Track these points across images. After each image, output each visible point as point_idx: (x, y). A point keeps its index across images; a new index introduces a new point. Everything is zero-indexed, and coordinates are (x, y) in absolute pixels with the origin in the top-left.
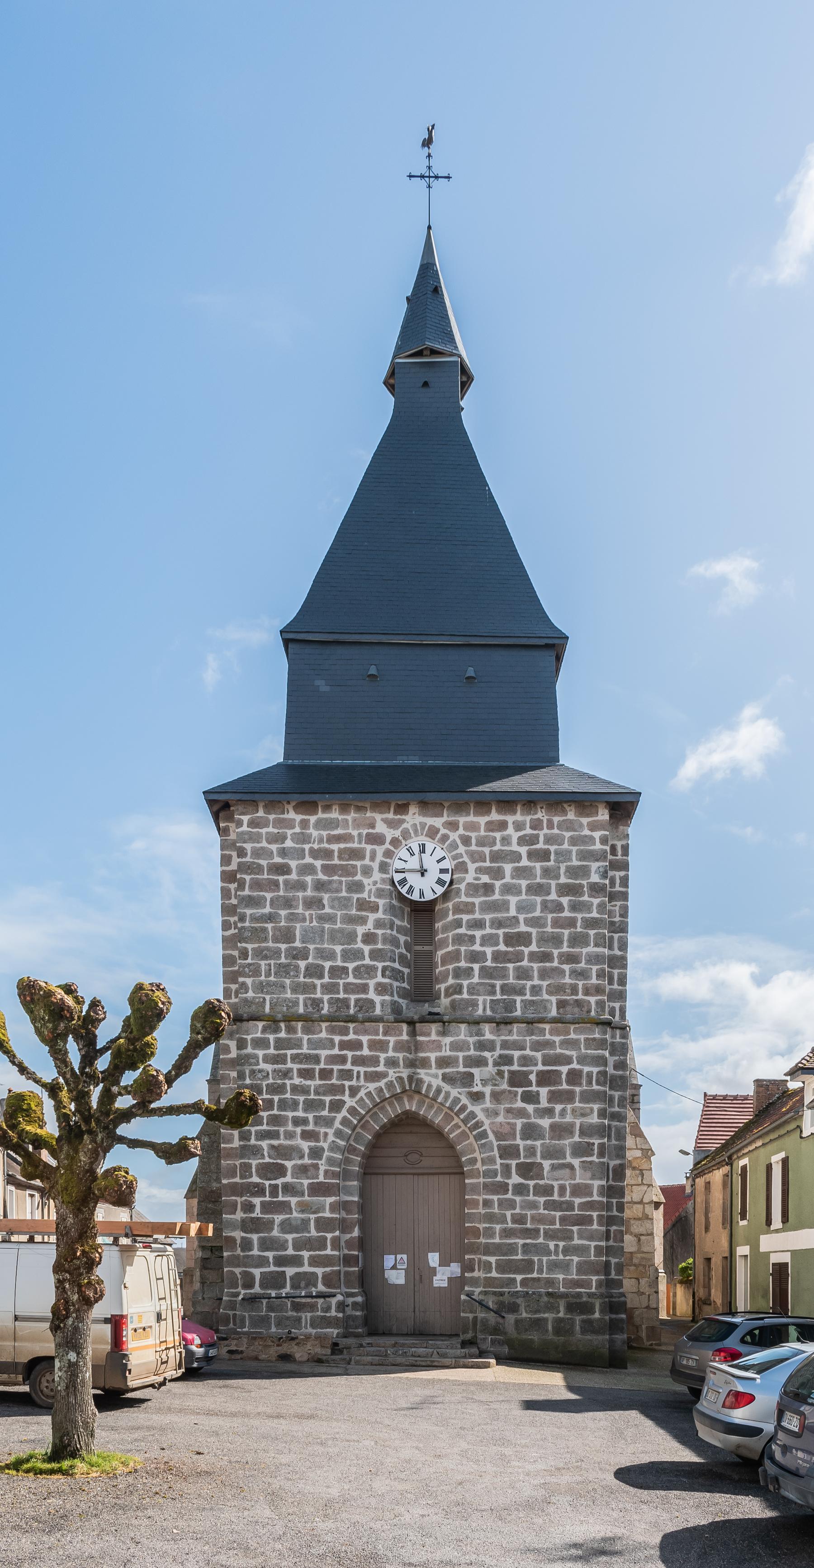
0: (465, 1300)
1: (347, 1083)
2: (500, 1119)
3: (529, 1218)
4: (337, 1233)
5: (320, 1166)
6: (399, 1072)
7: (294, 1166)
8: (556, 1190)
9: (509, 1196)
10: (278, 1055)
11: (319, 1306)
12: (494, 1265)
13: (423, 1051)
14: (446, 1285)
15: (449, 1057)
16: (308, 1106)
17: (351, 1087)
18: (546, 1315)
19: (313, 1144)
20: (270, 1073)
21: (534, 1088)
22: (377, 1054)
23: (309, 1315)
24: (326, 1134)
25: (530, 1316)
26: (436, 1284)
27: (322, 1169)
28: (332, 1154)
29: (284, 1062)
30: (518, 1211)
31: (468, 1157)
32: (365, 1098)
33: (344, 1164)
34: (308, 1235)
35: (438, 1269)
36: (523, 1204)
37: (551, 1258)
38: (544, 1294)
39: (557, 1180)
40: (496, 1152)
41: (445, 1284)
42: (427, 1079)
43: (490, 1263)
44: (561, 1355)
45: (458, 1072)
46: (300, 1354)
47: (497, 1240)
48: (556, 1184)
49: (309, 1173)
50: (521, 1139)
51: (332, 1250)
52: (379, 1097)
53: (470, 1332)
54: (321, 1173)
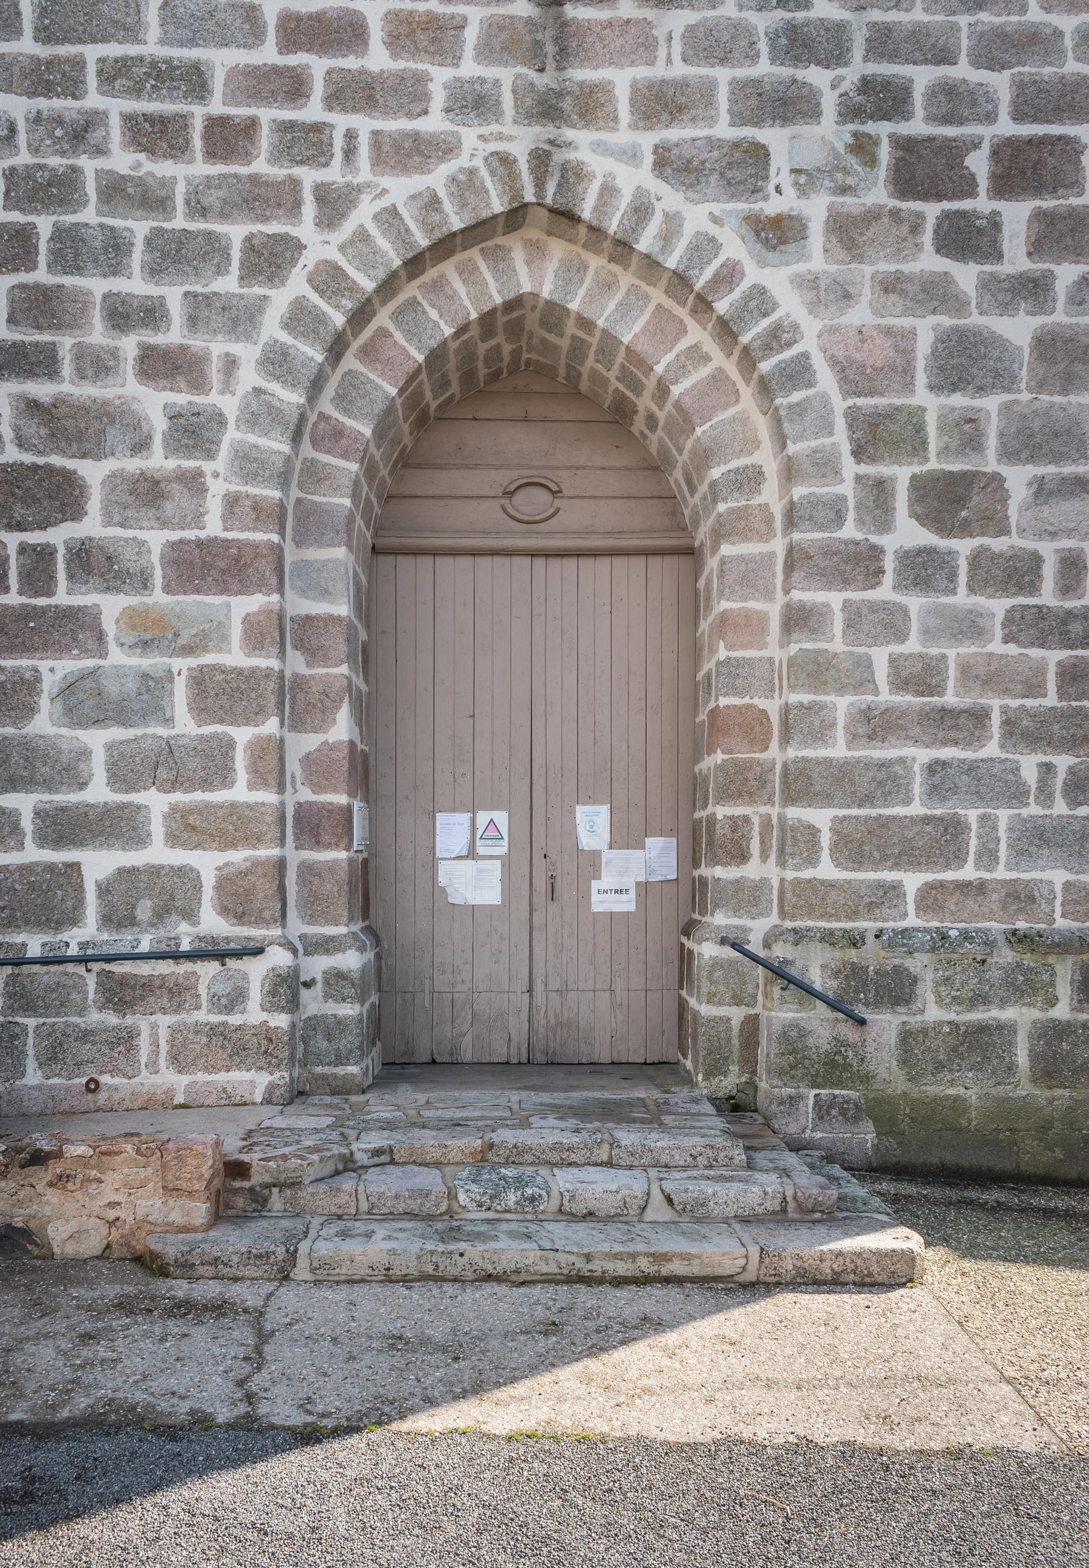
0: (716, 964)
1: (309, 176)
2: (860, 315)
3: (952, 672)
4: (271, 726)
5: (209, 481)
6: (500, 137)
7: (112, 480)
8: (1049, 571)
9: (885, 591)
10: (51, 63)
11: (202, 990)
12: (826, 839)
13: (589, 61)
14: (632, 907)
15: (682, 85)
16: (164, 255)
17: (323, 193)
18: (1008, 1014)
19: (181, 399)
20: (21, 126)
21: (982, 203)
22: (421, 66)
23: (164, 1021)
24: (231, 363)
25: (952, 1016)
26: (599, 903)
27: (217, 489)
28: (252, 438)
29: (74, 88)
30: (913, 645)
31: (734, 464)
32: (373, 229)
33: (301, 486)
34: (163, 732)
35: (607, 855)
36: (932, 622)
37: (1025, 812)
38: (1001, 939)
39: (1053, 535)
40: (841, 438)
41: (627, 904)
42: (598, 165)
43: (813, 831)
44: (1059, 1153)
45: (712, 143)
46: (69, 1228)
47: (838, 750)
48: (1048, 550)
49: (169, 507)
50: (931, 387)
51: (251, 787)
52: (427, 228)
53: (734, 1069)
54: (214, 506)
